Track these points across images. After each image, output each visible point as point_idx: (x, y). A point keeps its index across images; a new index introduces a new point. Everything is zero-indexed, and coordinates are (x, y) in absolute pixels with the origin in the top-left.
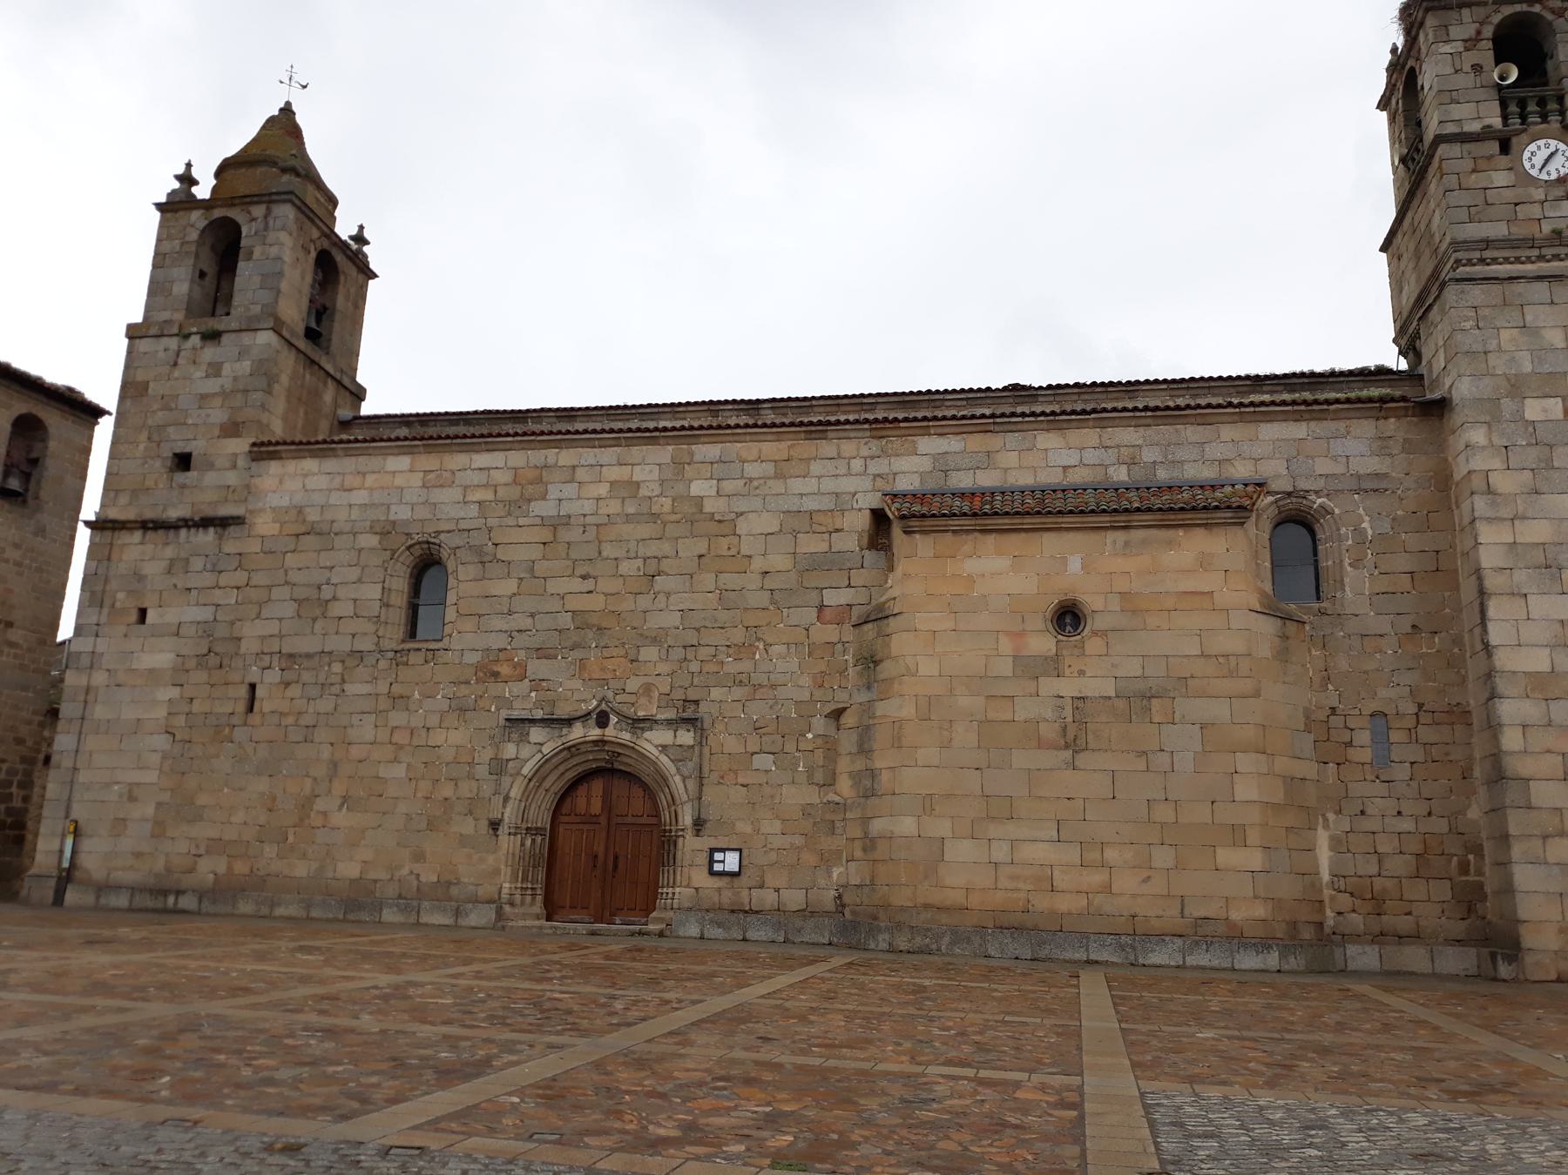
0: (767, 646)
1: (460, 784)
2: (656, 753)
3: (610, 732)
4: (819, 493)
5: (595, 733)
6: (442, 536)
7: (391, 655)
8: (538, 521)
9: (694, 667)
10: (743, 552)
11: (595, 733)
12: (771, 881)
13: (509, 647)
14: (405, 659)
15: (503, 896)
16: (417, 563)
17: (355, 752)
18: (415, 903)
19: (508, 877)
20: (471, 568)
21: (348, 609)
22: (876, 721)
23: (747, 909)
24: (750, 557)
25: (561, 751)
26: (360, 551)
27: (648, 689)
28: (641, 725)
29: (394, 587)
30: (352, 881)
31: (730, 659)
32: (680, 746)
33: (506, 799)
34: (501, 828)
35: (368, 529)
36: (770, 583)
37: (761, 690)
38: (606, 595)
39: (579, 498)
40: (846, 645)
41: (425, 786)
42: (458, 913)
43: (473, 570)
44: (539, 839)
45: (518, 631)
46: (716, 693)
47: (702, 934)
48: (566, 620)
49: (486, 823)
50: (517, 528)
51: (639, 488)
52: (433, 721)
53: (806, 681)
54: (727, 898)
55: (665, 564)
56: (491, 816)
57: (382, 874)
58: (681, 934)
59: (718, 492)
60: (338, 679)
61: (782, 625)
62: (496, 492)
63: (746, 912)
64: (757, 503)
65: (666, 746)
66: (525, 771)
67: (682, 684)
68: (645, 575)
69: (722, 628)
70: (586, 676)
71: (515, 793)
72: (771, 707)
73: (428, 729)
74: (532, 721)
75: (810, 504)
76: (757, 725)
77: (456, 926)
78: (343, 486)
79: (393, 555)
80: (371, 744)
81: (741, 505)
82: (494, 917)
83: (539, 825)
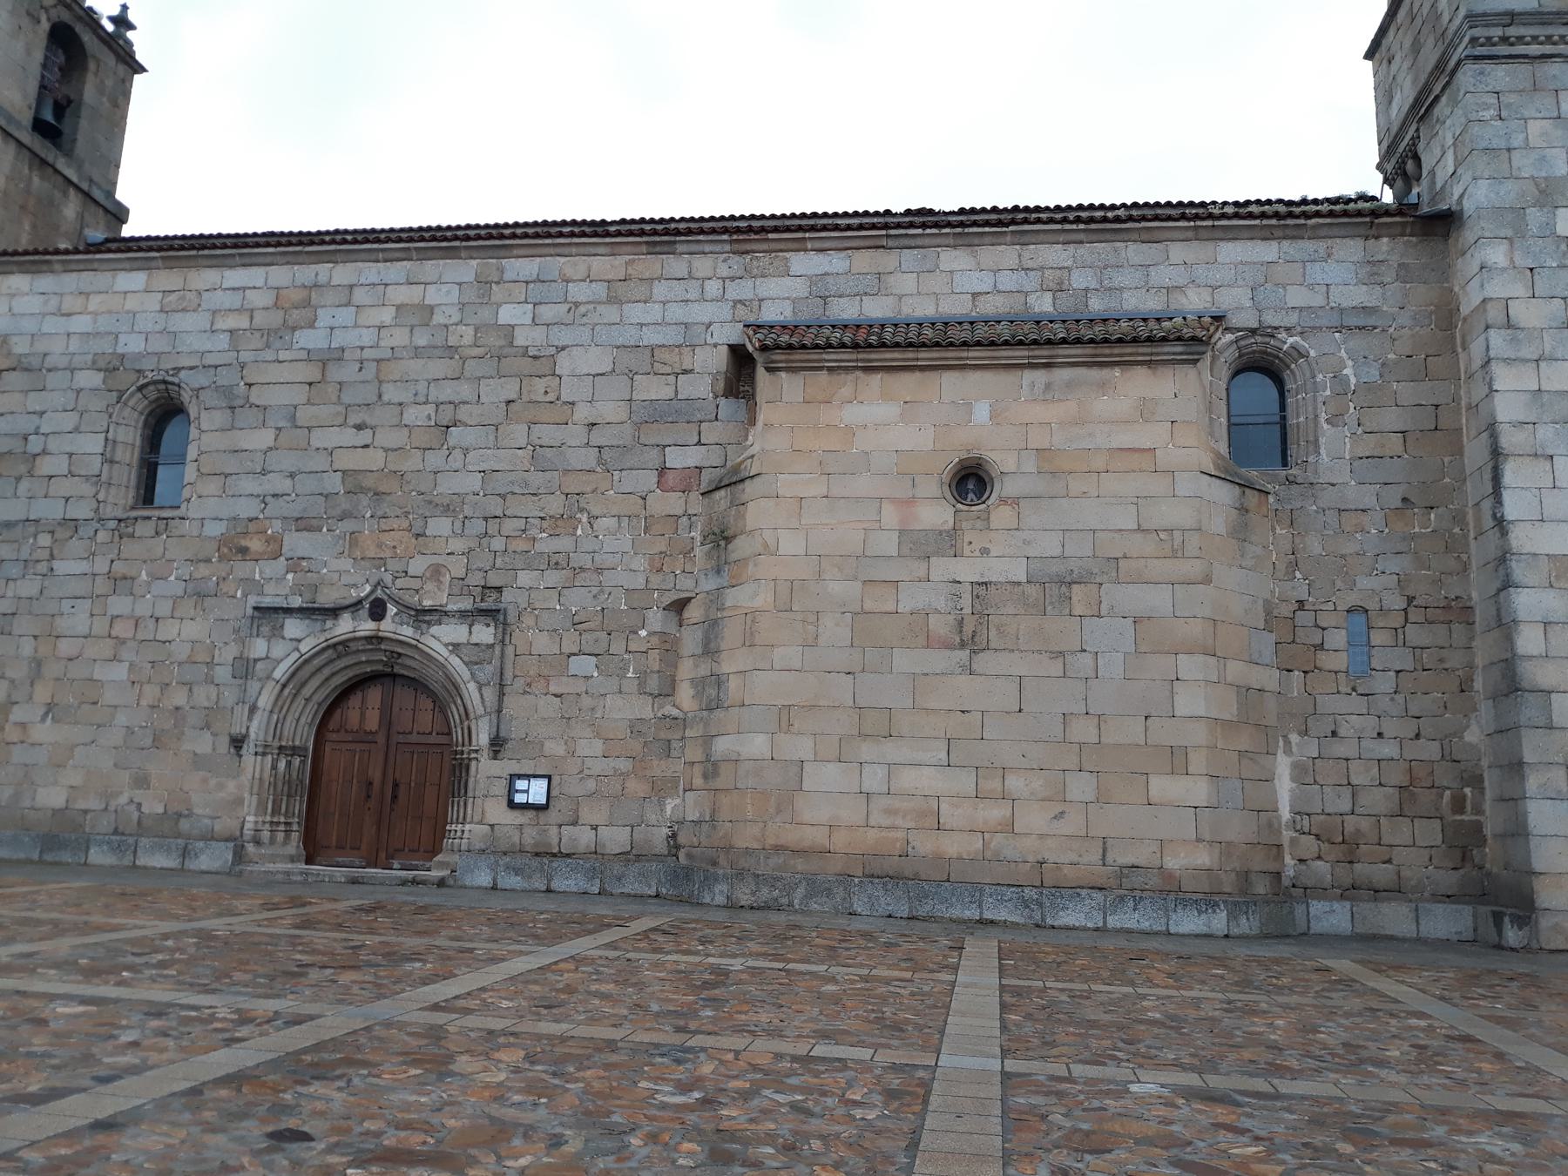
0: (593, 518)
1: (195, 689)
3: (387, 626)
5: (367, 627)
6: (183, 374)
7: (113, 524)
8: (303, 355)
9: (498, 544)
10: (564, 398)
11: (367, 627)
13: (261, 516)
14: (130, 530)
15: (245, 832)
17: (66, 648)
23: (555, 850)
24: (573, 404)
25: (324, 650)
26: (79, 392)
27: (436, 571)
28: (427, 618)
29: (120, 438)
30: (55, 812)
31: (544, 535)
32: (477, 644)
33: (253, 709)
34: (245, 746)
35: (89, 363)
36: (598, 438)
37: (583, 575)
39: (356, 326)
40: (693, 518)
41: (151, 693)
42: (185, 853)
43: (219, 418)
44: (297, 761)
45: (274, 496)
46: (525, 578)
48: (334, 483)
49: (227, 739)
52: (164, 609)
53: (640, 563)
54: (530, 837)
57: (94, 804)
58: (468, 883)
60: (45, 554)
62: (252, 318)
63: (554, 855)
64: (584, 335)
65: (459, 645)
66: (278, 674)
70: (358, 554)
71: (265, 701)
72: (595, 596)
73: (157, 620)
74: (288, 611)
75: (651, 337)
76: (577, 619)
78: (59, 310)
80: (85, 637)
81: (562, 336)
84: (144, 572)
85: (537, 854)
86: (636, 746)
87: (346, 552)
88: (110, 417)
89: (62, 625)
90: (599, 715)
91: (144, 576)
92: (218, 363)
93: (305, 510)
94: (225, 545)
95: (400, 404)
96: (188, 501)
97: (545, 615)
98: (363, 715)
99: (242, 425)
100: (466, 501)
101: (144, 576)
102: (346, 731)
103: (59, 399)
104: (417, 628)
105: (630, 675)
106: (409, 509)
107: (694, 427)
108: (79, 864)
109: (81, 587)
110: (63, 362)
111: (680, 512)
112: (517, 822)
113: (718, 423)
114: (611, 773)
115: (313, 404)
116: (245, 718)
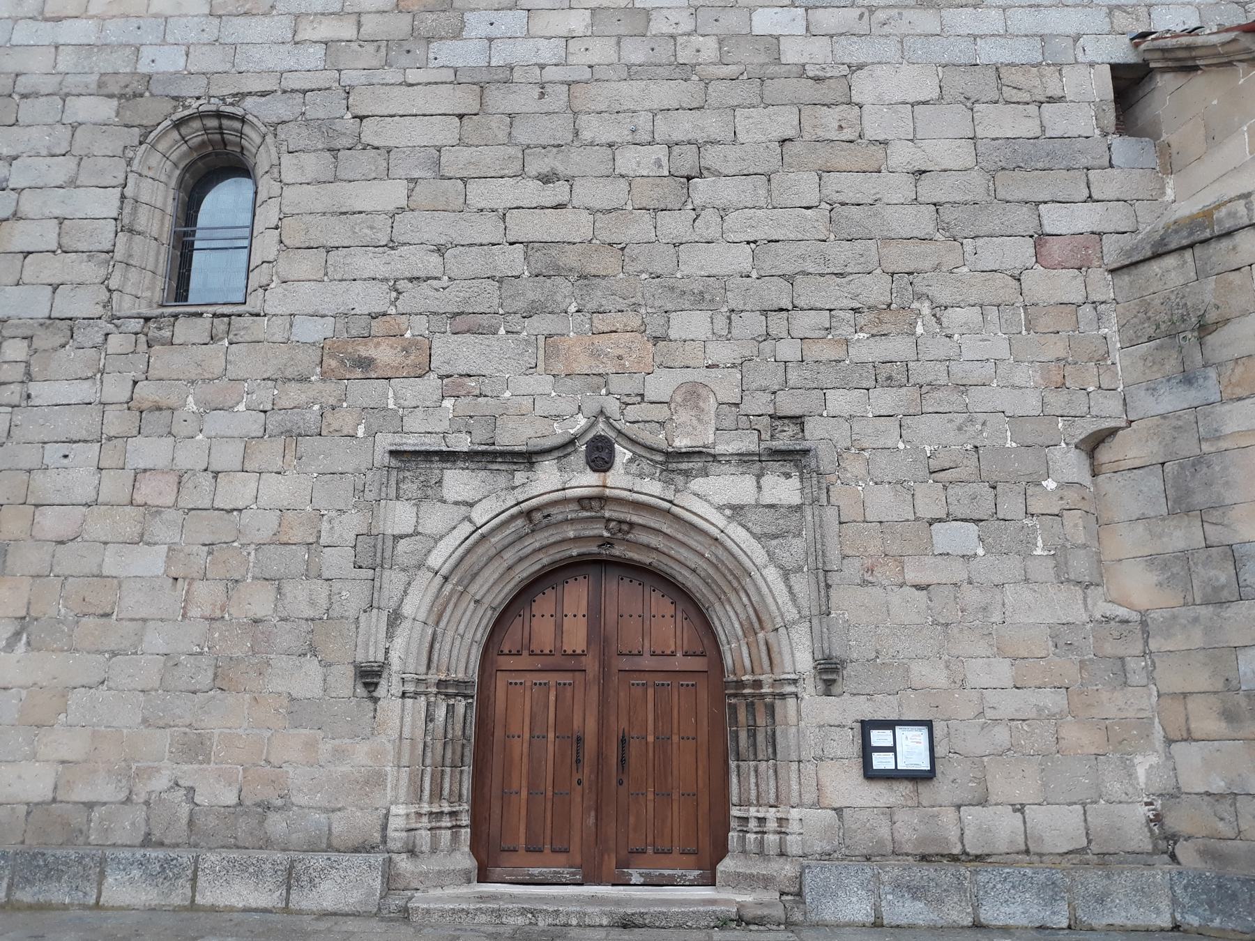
0: (939, 309)
1: (288, 588)
2: (720, 520)
3: (619, 479)
4: (1007, 34)
5: (585, 481)
6: (249, 102)
7: (136, 325)
8: (448, 75)
9: (787, 350)
10: (870, 134)
11: (585, 481)
12: (1000, 787)
13: (392, 311)
14: (166, 333)
15: (391, 833)
16: (193, 163)
17: (51, 523)
18: (186, 857)
19: (402, 792)
20: (309, 160)
21: (42, 235)
22: (1223, 445)
23: (956, 850)
24: (885, 143)
25: (513, 518)
26: (74, 127)
27: (693, 394)
28: (684, 466)
29: (144, 198)
30: (31, 807)
31: (862, 335)
32: (772, 506)
33: (395, 618)
34: (383, 682)
35: (93, 86)
36: (930, 190)
37: (936, 394)
38: (592, 211)
39: (528, 36)
40: (1102, 308)
41: (206, 595)
42: (290, 878)
43: (314, 164)
44: (461, 706)
45: (411, 280)
46: (839, 401)
47: (878, 916)
48: (512, 261)
49: (350, 672)
50: (404, 88)
51: (649, 21)
52: (227, 456)
53: (1024, 375)
54: (909, 829)
55: (712, 157)
56: (360, 658)
57: (106, 791)
58: (828, 916)
59: (807, 29)
60: (18, 372)
61: (965, 269)
62: (359, 25)
63: (954, 858)
64: (890, 50)
65: (742, 507)
66: (435, 560)
67: (764, 383)
68: (671, 175)
69: (841, 275)
70: (559, 368)
71: (416, 604)
72: (960, 429)
73: (216, 474)
74: (449, 457)
75: (989, 52)
76: (934, 464)
77: (286, 910)
78: (42, 13)
79: (146, 136)
80: (88, 505)
81: (856, 52)
82: (378, 884)
83: (461, 676)
84: (190, 399)
85: (924, 858)
86: (1068, 669)
87: (541, 365)
88: (129, 164)
89: (45, 485)
90: (996, 617)
91: (191, 404)
92: (307, 87)
93: (466, 301)
94: (332, 356)
95: (610, 146)
96: (265, 288)
97: (882, 459)
98: (559, 628)
99: (351, 176)
100: (730, 285)
101: (191, 404)
102: (532, 653)
103: (39, 138)
104: (668, 482)
105: (1038, 552)
106: (639, 299)
107: (1080, 175)
108: (85, 907)
109: (82, 424)
110: (50, 84)
111: (1079, 299)
112: (882, 802)
113: (1115, 171)
114: (1034, 715)
115: (468, 146)
116: (382, 634)
